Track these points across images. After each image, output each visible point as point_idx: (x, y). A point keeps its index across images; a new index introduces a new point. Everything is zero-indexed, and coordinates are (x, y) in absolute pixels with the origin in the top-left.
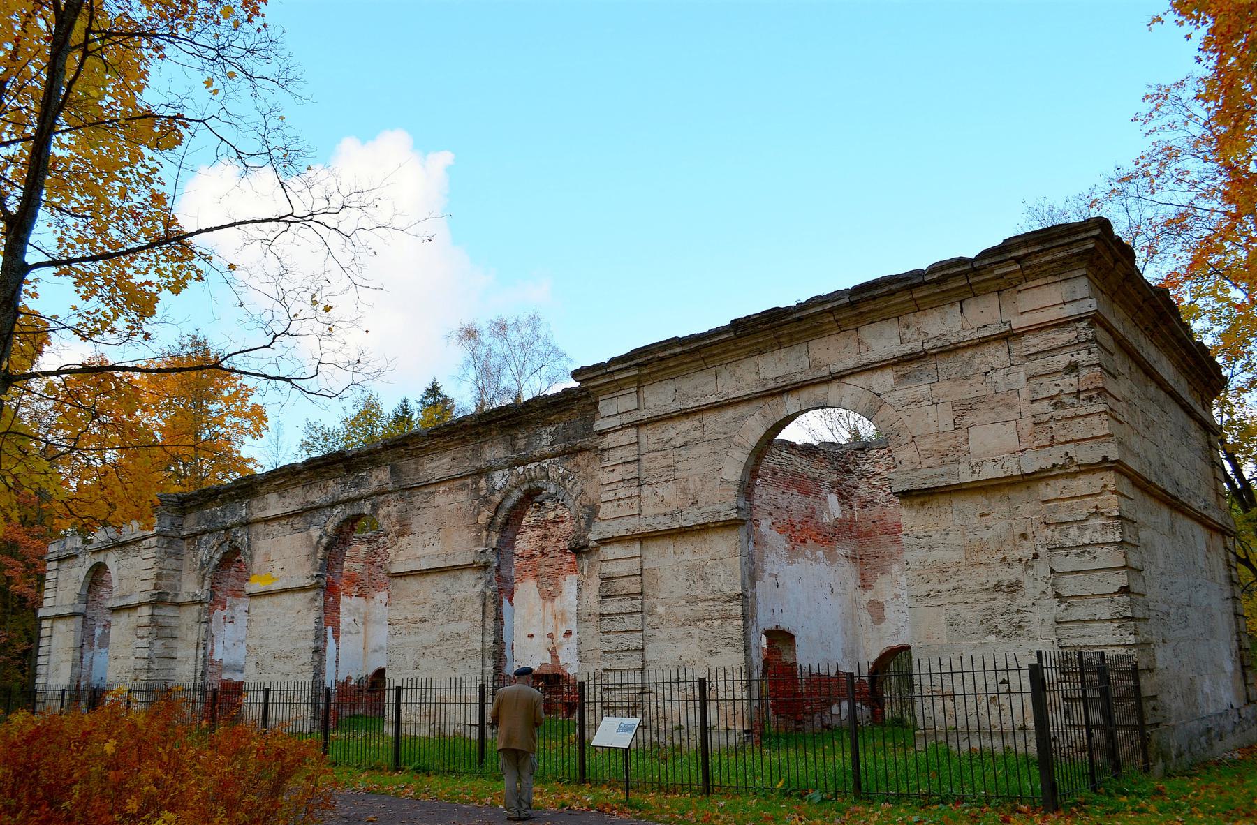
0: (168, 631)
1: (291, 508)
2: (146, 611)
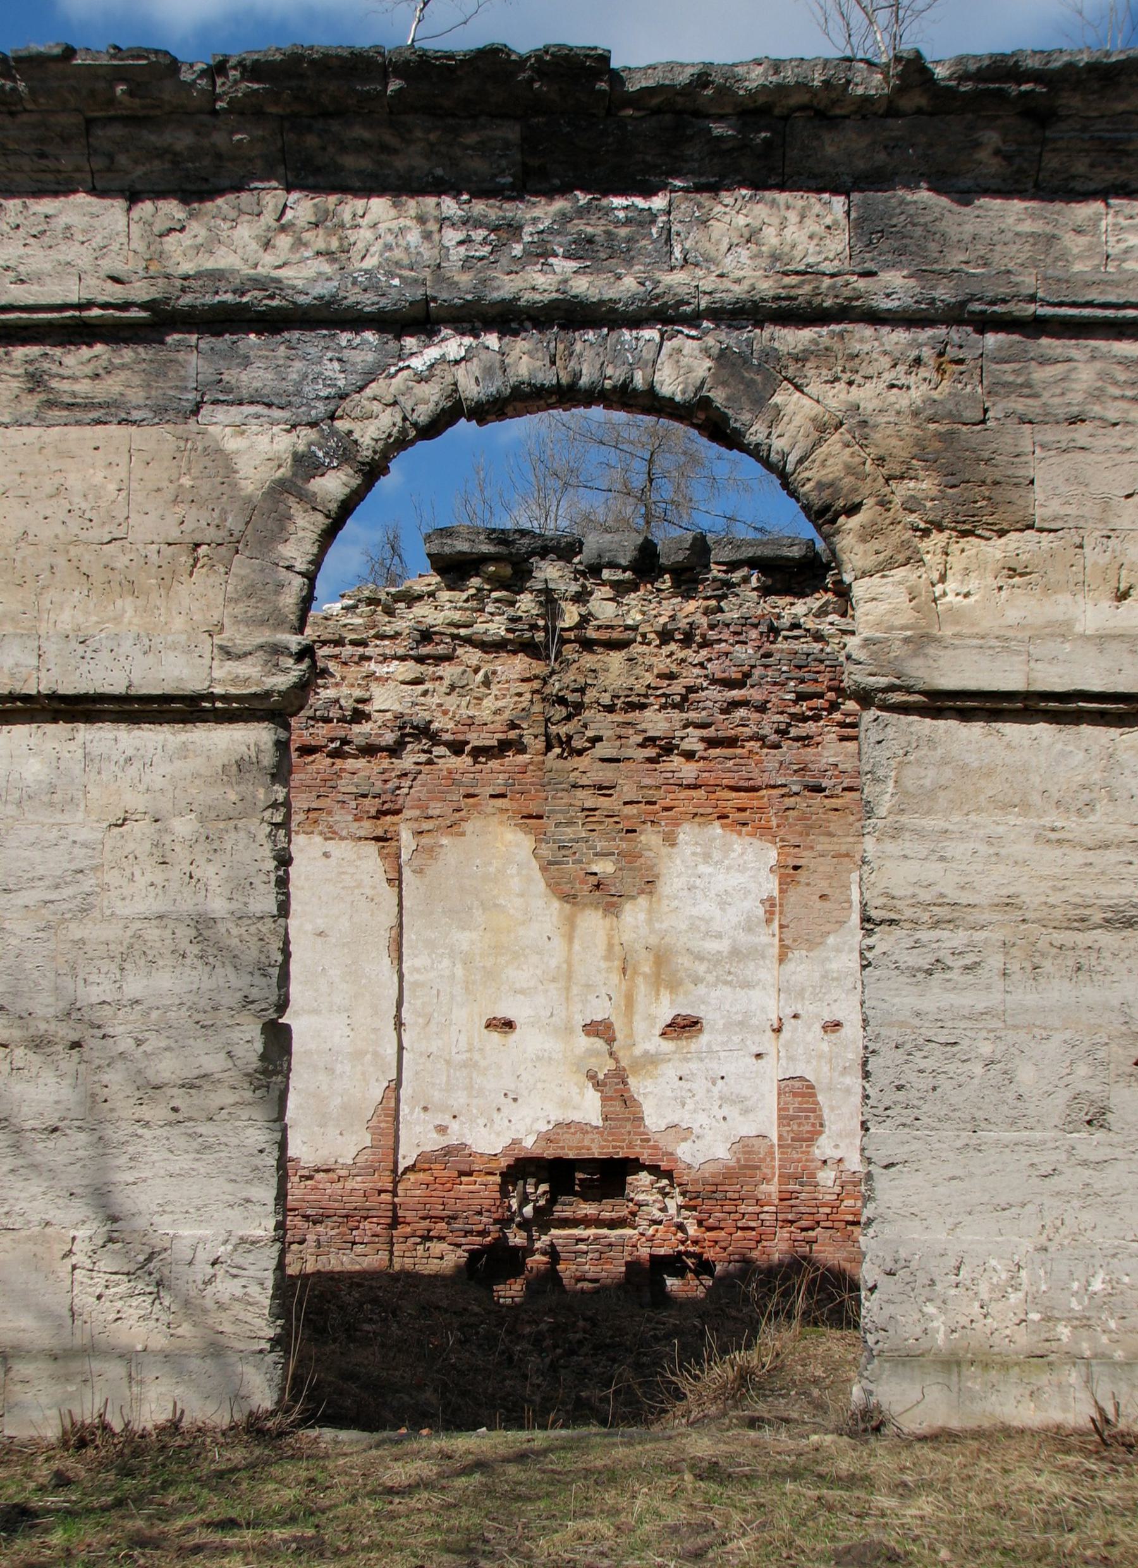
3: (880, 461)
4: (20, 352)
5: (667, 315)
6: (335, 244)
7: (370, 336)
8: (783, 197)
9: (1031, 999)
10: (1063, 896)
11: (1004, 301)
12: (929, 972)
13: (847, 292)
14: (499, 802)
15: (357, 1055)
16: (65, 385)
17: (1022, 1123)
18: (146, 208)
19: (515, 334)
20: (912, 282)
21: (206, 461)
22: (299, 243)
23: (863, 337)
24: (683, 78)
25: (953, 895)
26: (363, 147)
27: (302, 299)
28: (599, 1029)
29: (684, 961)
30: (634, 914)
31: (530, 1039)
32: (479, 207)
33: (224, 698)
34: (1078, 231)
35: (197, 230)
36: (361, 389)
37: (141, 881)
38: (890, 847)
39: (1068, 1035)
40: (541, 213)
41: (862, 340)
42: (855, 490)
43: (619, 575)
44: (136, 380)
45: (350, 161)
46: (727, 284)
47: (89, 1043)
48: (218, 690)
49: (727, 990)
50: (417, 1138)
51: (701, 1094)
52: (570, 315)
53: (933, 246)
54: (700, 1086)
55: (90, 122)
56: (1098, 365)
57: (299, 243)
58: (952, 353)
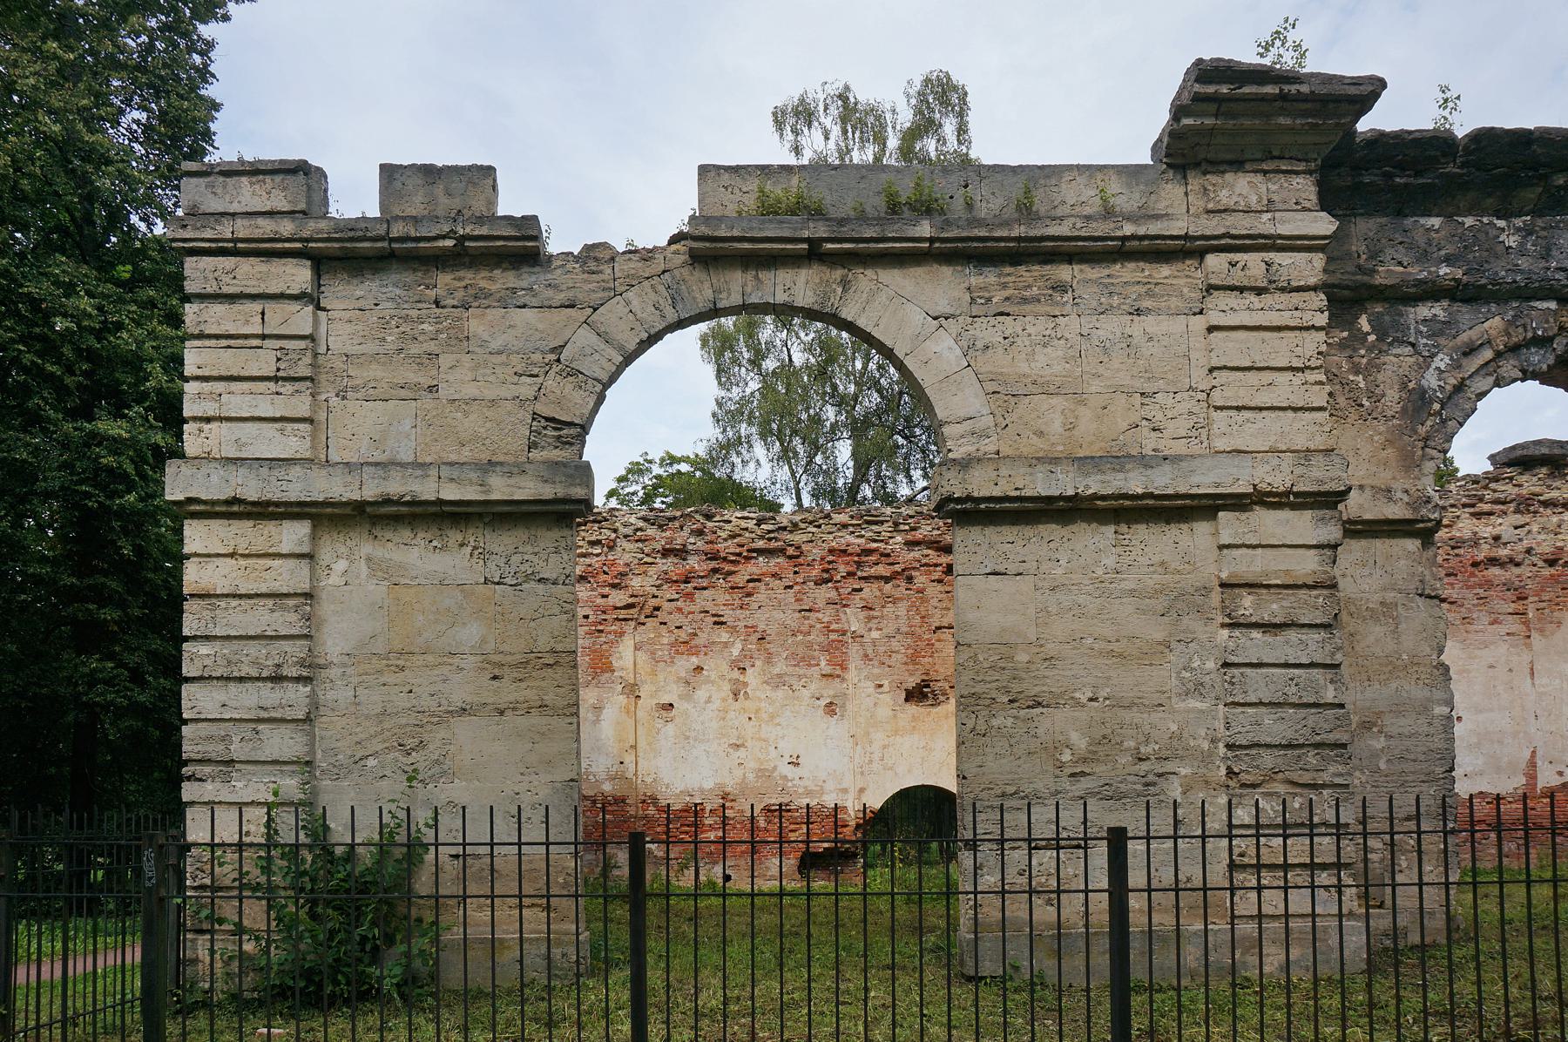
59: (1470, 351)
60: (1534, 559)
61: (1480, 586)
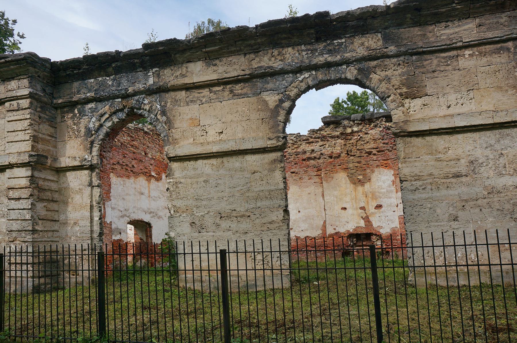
0: (48, 194)
1: (234, 74)
2: (24, 172)
3: (393, 86)
4: (228, 86)
5: (348, 62)
6: (282, 58)
7: (291, 75)
8: (367, 35)
9: (438, 194)
10: (443, 172)
11: (415, 49)
12: (415, 190)
13: (383, 52)
14: (340, 167)
15: (318, 216)
16: (236, 92)
17: (439, 221)
18: (248, 56)
19: (318, 70)
20: (396, 48)
21: (263, 103)
22: (276, 59)
23: (387, 62)
24: (344, 14)
25: (419, 174)
26: (285, 38)
27: (277, 69)
28: (363, 208)
29: (377, 194)
30: (367, 186)
31: (349, 211)
32: (309, 47)
33: (270, 147)
34: (430, 32)
35: (257, 59)
36: (290, 85)
37: (258, 184)
38: (404, 165)
39: (447, 201)
40: (321, 46)
41: (387, 62)
42: (388, 93)
43: (358, 122)
44: (249, 89)
45: (283, 41)
46: (358, 54)
47: (251, 216)
48: (268, 146)
49: (386, 199)
50: (330, 231)
51: (383, 220)
52: (328, 65)
53: (400, 40)
54: (383, 218)
55: (235, 42)
56: (438, 59)
57: (276, 59)
58: (406, 61)
59: (102, 115)
60: (325, 157)
61: (305, 167)
